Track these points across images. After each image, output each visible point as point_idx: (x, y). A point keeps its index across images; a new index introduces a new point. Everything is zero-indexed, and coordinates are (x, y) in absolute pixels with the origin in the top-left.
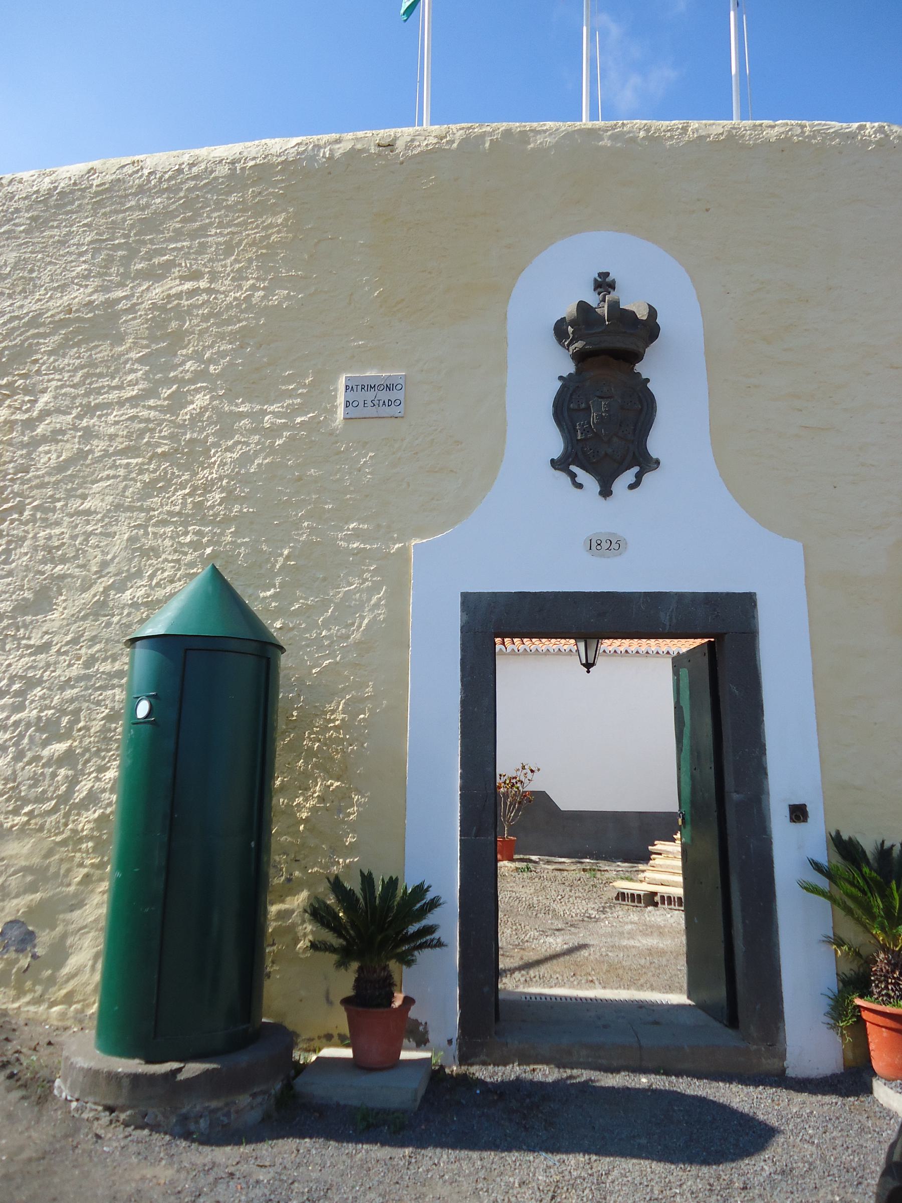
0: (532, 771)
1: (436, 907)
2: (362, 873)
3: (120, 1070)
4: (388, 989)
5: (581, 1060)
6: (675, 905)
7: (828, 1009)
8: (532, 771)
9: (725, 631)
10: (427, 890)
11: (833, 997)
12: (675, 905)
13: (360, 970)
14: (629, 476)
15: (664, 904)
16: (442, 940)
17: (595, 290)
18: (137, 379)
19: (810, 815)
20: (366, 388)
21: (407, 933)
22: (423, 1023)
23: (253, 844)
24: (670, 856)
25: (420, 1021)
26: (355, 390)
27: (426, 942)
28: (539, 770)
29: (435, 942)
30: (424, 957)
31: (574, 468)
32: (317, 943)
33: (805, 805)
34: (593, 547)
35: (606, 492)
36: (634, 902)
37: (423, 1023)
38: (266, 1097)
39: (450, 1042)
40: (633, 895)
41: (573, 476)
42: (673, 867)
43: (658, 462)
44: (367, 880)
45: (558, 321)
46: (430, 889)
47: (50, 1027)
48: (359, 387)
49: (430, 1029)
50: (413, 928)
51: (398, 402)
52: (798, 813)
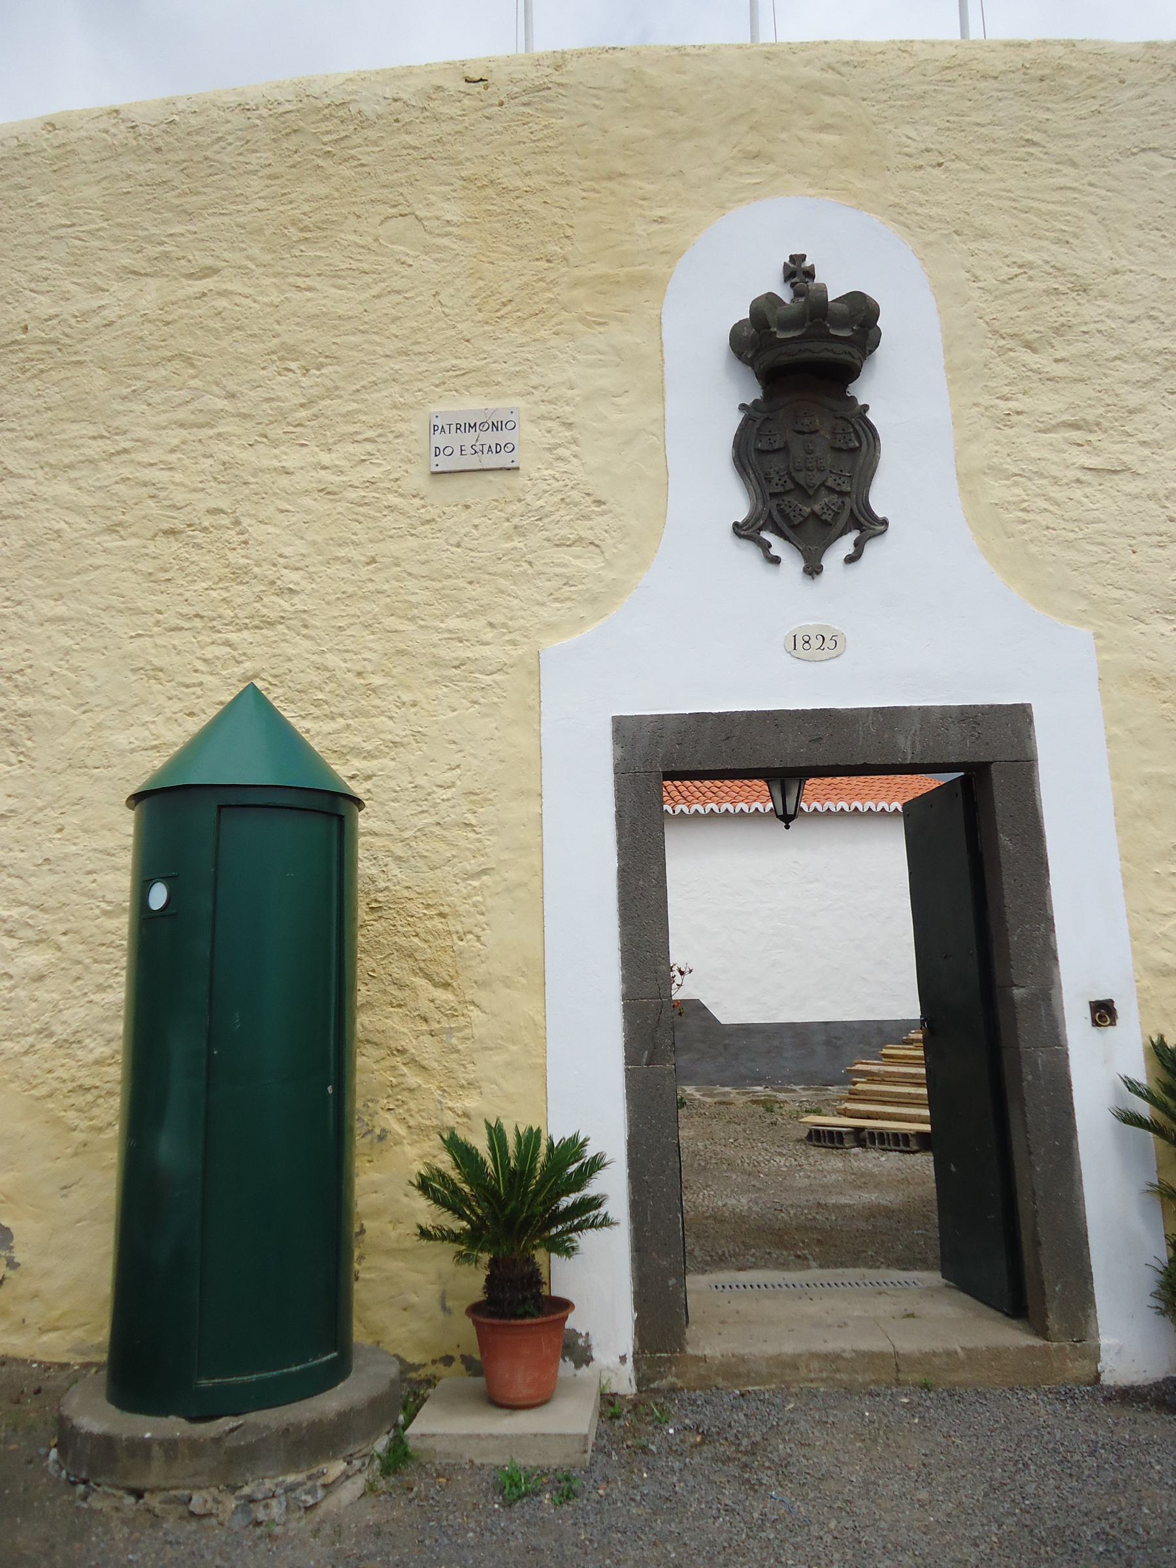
0: (682, 973)
1: (600, 1169)
2: (488, 1125)
3: (148, 1435)
4: (534, 1291)
5: (812, 1375)
6: (889, 1144)
7: (1155, 1287)
8: (682, 973)
9: (990, 760)
10: (583, 1145)
11: (1162, 1269)
12: (889, 1144)
13: (493, 1264)
14: (846, 544)
15: (874, 1144)
16: (610, 1215)
17: (785, 281)
18: (76, 1126)
19: (1119, 1013)
20: (463, 428)
21: (558, 1208)
22: (584, 1334)
23: (330, 1089)
24: (875, 1078)
25: (578, 1331)
26: (447, 430)
27: (587, 1219)
28: (691, 971)
29: (600, 1219)
30: (587, 1240)
31: (767, 536)
32: (430, 1229)
33: (1112, 1001)
34: (799, 646)
35: (813, 569)
36: (820, 1141)
37: (584, 1334)
38: (367, 1462)
39: (623, 1359)
40: (830, 1132)
41: (765, 546)
42: (918, 1096)
43: (885, 522)
44: (496, 1134)
45: (736, 325)
46: (588, 1142)
47: (39, 1366)
48: (453, 428)
49: (593, 1342)
50: (566, 1202)
51: (510, 447)
52: (1103, 1012)
